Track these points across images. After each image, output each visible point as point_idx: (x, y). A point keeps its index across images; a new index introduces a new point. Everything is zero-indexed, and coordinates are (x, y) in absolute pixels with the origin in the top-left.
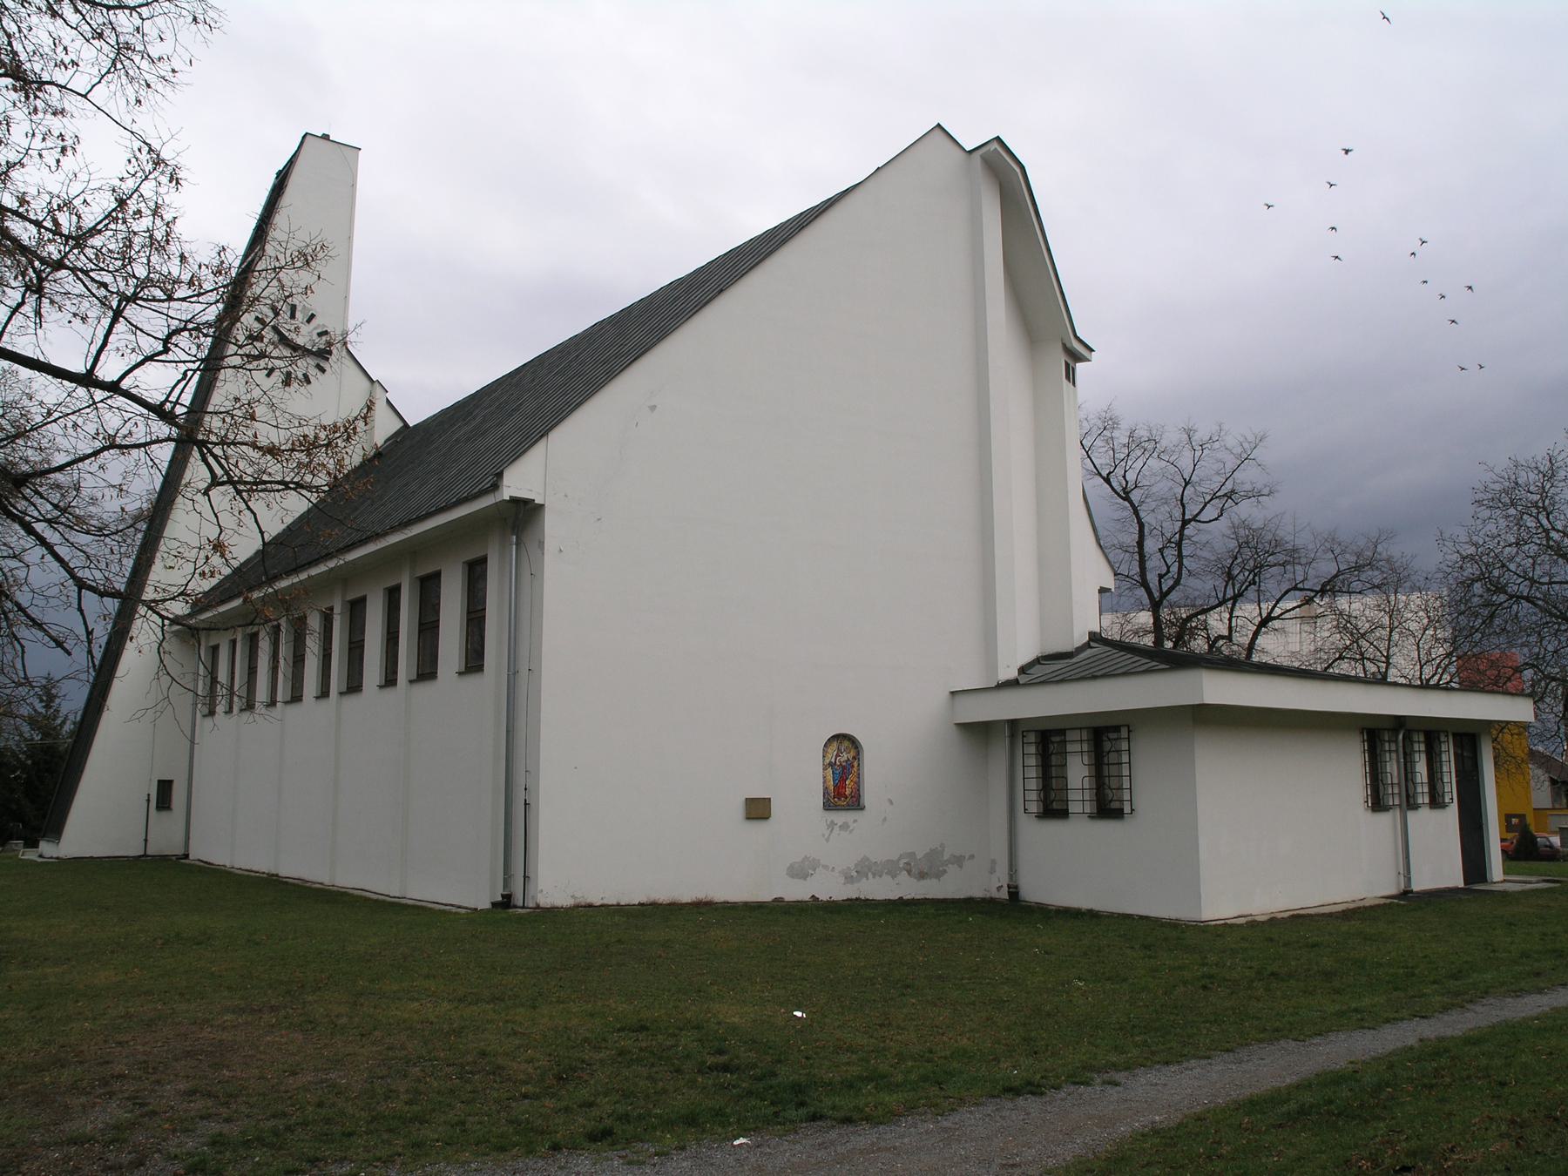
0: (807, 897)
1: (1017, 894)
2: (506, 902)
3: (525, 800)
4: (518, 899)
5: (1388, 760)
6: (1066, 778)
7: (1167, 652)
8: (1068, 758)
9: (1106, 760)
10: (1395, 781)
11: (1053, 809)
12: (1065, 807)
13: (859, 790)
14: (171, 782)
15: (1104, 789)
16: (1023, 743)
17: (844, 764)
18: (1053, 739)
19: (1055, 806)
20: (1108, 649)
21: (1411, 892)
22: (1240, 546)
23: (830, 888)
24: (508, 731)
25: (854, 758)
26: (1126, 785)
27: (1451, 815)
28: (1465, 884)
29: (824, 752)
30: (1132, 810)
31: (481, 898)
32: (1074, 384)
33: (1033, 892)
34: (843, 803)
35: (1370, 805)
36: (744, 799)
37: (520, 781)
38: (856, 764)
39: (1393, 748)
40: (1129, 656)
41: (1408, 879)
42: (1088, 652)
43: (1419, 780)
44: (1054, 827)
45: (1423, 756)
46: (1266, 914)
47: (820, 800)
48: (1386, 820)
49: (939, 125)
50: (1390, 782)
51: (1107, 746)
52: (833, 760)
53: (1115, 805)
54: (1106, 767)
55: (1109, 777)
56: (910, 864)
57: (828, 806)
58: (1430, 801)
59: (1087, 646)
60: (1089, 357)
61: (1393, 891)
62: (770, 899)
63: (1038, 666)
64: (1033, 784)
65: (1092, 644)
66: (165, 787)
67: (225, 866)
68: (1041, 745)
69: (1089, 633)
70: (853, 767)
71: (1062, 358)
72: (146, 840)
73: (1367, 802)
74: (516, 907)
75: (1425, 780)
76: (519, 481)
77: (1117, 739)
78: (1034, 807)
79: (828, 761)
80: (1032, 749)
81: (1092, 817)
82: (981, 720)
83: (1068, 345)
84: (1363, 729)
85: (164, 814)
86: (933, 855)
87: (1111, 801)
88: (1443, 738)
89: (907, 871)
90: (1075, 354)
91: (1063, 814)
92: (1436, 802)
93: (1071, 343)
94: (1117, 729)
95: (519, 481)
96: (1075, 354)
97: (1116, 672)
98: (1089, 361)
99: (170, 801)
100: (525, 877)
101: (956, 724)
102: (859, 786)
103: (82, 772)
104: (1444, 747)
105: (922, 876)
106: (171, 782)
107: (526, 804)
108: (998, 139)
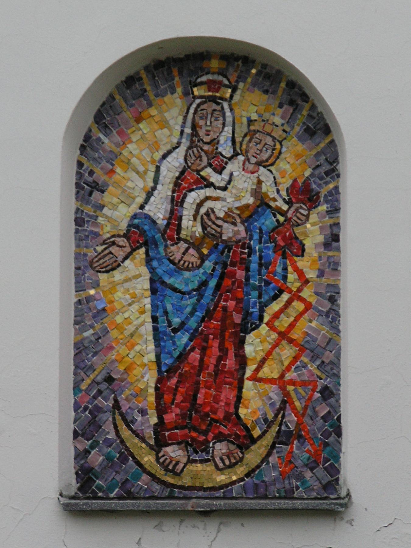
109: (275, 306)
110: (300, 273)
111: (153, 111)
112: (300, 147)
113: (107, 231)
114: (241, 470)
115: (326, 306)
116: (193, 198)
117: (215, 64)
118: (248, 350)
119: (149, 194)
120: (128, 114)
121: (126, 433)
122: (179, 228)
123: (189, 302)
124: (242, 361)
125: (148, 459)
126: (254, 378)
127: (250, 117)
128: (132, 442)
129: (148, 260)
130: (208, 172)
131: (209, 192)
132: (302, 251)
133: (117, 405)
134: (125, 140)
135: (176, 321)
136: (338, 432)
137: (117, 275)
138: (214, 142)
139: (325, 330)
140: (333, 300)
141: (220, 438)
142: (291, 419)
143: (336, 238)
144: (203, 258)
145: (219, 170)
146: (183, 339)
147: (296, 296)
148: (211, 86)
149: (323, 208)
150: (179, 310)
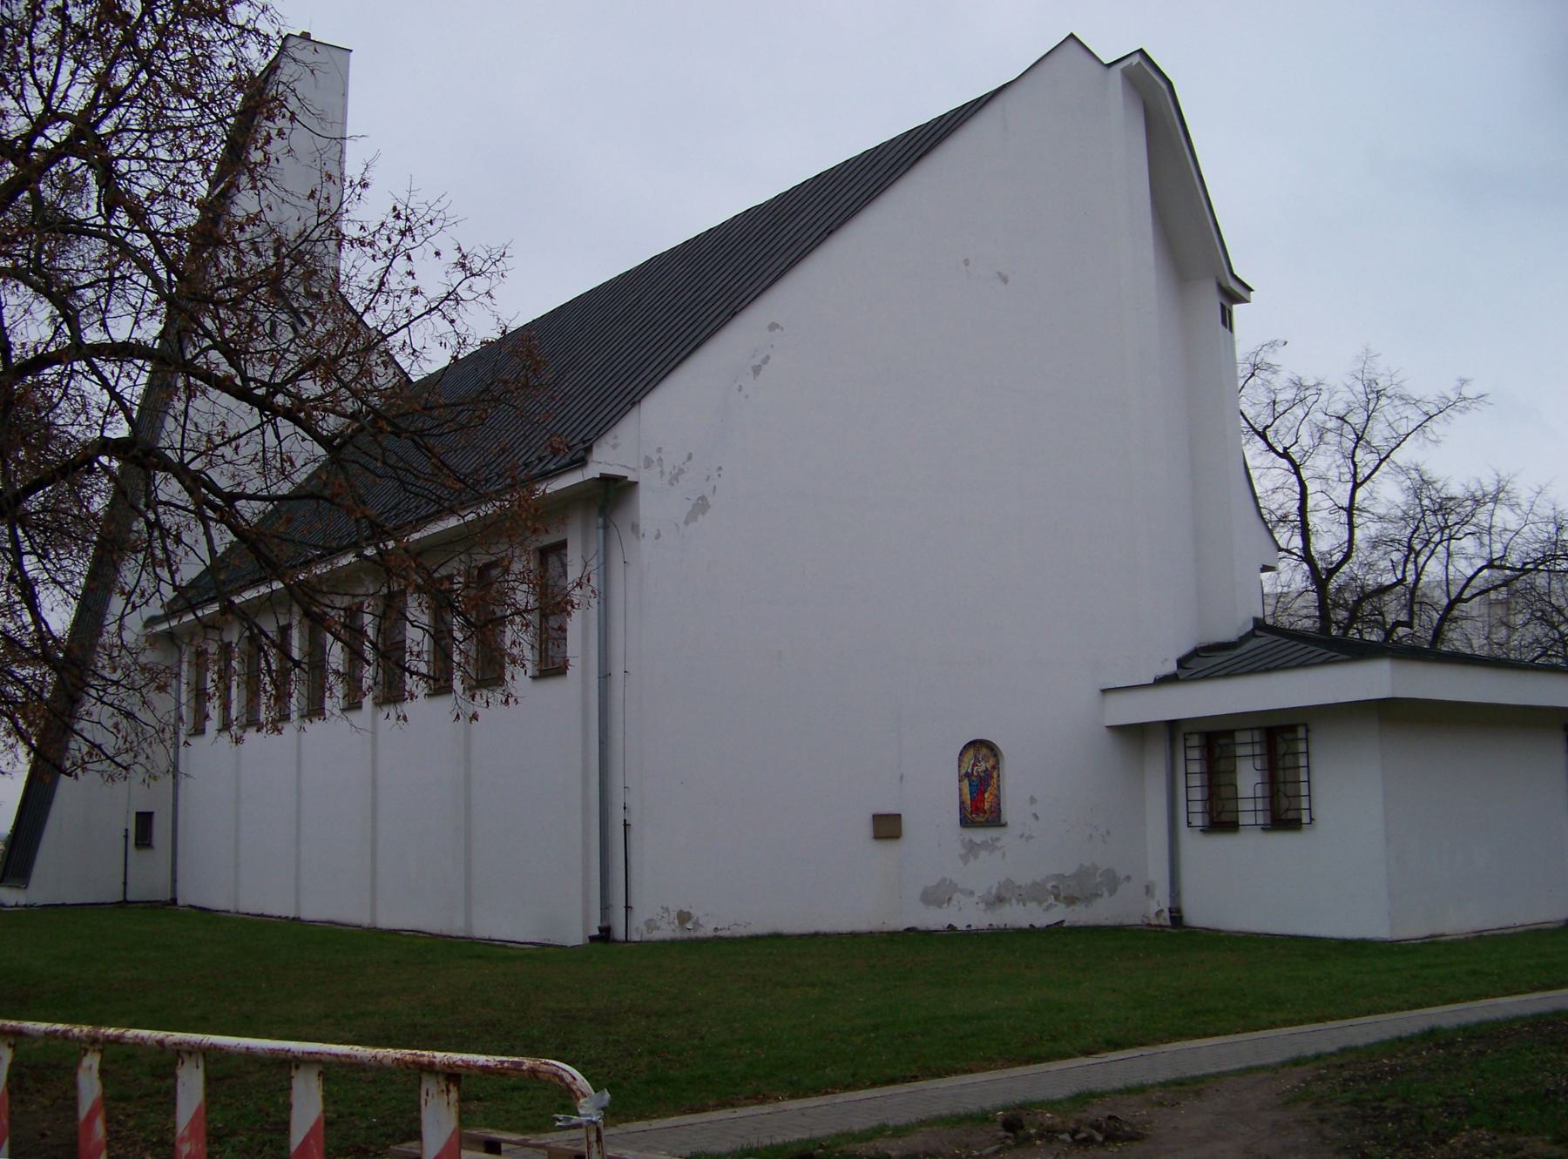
0: (1026, 925)
1: (1181, 918)
2: (605, 935)
3: (625, 821)
4: (619, 933)
7: (1335, 638)
9: (1280, 764)
11: (1221, 821)
13: (999, 804)
14: (151, 814)
16: (1185, 747)
17: (982, 774)
19: (1225, 818)
20: (1275, 638)
23: (968, 915)
24: (601, 742)
25: (994, 767)
29: (960, 760)
30: (1312, 819)
31: (574, 933)
32: (1231, 330)
33: (1196, 915)
34: (981, 819)
36: (870, 816)
37: (617, 798)
38: (995, 775)
40: (1302, 646)
42: (1254, 643)
44: (1222, 843)
47: (956, 816)
49: (1072, 36)
51: (1282, 748)
52: (969, 771)
53: (1291, 815)
54: (1281, 773)
57: (965, 822)
59: (1251, 635)
60: (1246, 298)
63: (1196, 660)
64: (1197, 794)
65: (1258, 633)
66: (145, 820)
67: (228, 912)
70: (992, 777)
71: (1214, 300)
72: (125, 883)
74: (615, 941)
76: (606, 460)
78: (1198, 820)
79: (963, 771)
80: (1195, 754)
82: (1133, 722)
83: (1224, 285)
85: (145, 853)
87: (1288, 810)
89: (1054, 894)
90: (1233, 293)
91: (1231, 826)
93: (1227, 283)
94: (1292, 728)
95: (606, 460)
96: (1233, 293)
97: (1289, 664)
98: (1247, 302)
99: (151, 837)
100: (627, 907)
103: (50, 803)
105: (1071, 901)
106: (151, 814)
107: (625, 825)
108: (1141, 51)
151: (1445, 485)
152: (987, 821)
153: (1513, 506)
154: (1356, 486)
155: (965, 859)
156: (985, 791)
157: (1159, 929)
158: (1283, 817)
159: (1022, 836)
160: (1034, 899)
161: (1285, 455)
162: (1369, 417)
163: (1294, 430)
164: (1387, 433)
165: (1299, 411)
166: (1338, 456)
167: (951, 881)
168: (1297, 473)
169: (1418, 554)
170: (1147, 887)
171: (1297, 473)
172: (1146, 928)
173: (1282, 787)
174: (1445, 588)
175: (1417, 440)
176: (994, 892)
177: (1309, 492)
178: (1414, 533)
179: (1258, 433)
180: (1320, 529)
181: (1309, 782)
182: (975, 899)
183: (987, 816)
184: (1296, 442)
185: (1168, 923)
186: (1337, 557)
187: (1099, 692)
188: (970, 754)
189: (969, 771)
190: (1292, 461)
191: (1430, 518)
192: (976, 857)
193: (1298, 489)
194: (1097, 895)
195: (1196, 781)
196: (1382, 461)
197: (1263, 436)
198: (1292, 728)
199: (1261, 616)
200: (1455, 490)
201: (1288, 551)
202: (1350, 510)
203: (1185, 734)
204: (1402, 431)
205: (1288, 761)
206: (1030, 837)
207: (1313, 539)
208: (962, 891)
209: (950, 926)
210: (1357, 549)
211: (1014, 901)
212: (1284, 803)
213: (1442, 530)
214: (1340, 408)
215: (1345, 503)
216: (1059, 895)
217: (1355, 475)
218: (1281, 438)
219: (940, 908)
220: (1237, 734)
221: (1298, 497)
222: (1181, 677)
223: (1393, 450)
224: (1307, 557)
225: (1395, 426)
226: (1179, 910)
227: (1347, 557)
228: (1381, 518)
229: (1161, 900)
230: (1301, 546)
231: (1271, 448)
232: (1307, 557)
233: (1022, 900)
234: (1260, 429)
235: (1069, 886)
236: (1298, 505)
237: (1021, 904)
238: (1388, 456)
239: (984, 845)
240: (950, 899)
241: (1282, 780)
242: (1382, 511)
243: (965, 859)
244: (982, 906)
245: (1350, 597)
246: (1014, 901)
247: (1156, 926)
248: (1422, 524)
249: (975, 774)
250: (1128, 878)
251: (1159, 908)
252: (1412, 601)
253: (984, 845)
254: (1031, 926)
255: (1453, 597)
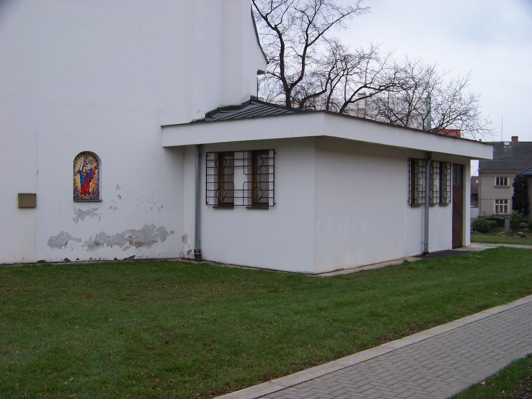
0: (112, 258)
1: (200, 255)
5: (421, 177)
6: (233, 183)
8: (235, 170)
9: (259, 172)
10: (424, 190)
12: (231, 202)
13: (98, 189)
15: (257, 190)
16: (207, 160)
17: (88, 172)
18: (226, 158)
19: (226, 200)
21: (428, 253)
22: (336, 61)
25: (96, 168)
26: (271, 187)
27: (449, 209)
28: (453, 248)
30: (274, 204)
34: (87, 197)
35: (410, 203)
38: (96, 172)
39: (424, 170)
41: (426, 245)
42: (250, 107)
43: (435, 190)
44: (224, 214)
45: (438, 176)
46: (352, 269)
48: (418, 212)
50: (421, 190)
51: (260, 163)
52: (81, 169)
53: (263, 200)
54: (259, 177)
55: (260, 182)
56: (132, 237)
57: (77, 199)
58: (440, 202)
59: (249, 103)
61: (419, 252)
62: (35, 261)
63: (218, 114)
64: (212, 187)
65: (252, 102)
68: (218, 162)
69: (251, 96)
70: (95, 173)
73: (409, 201)
75: (438, 190)
77: (266, 158)
78: (212, 201)
79: (77, 170)
80: (212, 164)
81: (249, 208)
84: (409, 158)
86: (147, 230)
87: (261, 198)
88: (448, 167)
91: (230, 206)
92: (442, 203)
94: (267, 152)
101: (167, 148)
102: (98, 186)
104: (448, 172)
105: (139, 244)
109: (93, 180)
110: (95, 176)
111: (81, 158)
112: (95, 163)
113: (76, 172)
114: (90, 197)
115: (98, 180)
116: (84, 168)
117: (87, 154)
118: (90, 184)
119: (80, 167)
120: (78, 158)
121: (78, 193)
122: (83, 171)
123: (84, 179)
124: (89, 185)
125: (80, 196)
126: (91, 187)
127: (517, 137)
128: (78, 194)
129: (80, 174)
130: (86, 165)
131: (86, 167)
132: (95, 174)
133: (77, 190)
134: (78, 161)
135: (83, 181)
136: (99, 193)
137: (77, 176)
138: (87, 162)
139: (98, 182)
140: (99, 179)
141: (87, 194)
142: (94, 191)
143: (99, 173)
144: (85, 174)
145: (87, 165)
146: (83, 183)
147: (95, 179)
148: (86, 156)
149: (97, 169)
150: (83, 180)
151: (347, 48)
152: (91, 198)
153: (377, 60)
154: (307, 46)
155: (76, 220)
156: (90, 181)
157: (188, 261)
158: (259, 201)
159: (111, 208)
160: (118, 243)
161: (275, 28)
162: (316, 13)
163: (280, 17)
164: (323, 22)
165: (283, 7)
166: (300, 31)
167: (67, 233)
168: (280, 37)
169: (332, 81)
170: (183, 237)
171: (280, 37)
172: (180, 260)
173: (259, 184)
174: (344, 96)
175: (336, 26)
176: (93, 239)
177: (285, 47)
178: (332, 69)
179: (263, 17)
180: (289, 65)
181: (274, 182)
182: (82, 243)
183: (90, 196)
184: (281, 22)
185: (194, 258)
186: (296, 79)
187: (159, 128)
188: (82, 159)
189: (81, 169)
190: (278, 32)
191: (339, 64)
192: (83, 219)
193: (280, 45)
194: (154, 242)
195: (212, 179)
196: (319, 35)
197: (266, 19)
198: (267, 152)
199: (256, 96)
200: (352, 51)
201: (274, 74)
202: (303, 57)
203: (207, 153)
204: (330, 22)
205: (263, 170)
206: (116, 208)
207: (285, 70)
208: (74, 239)
209: (66, 259)
210: (306, 75)
211: (105, 245)
212: (260, 194)
213: (344, 70)
214: (302, 7)
215: (301, 54)
216: (132, 241)
217: (307, 41)
218: (274, 20)
219: (61, 249)
220: (235, 153)
221: (280, 49)
222: (206, 120)
223: (325, 30)
224: (282, 77)
225: (327, 19)
226: (200, 251)
227: (300, 79)
228: (317, 62)
229: (190, 245)
230: (280, 72)
231: (270, 25)
232: (282, 77)
233: (110, 244)
234: (265, 15)
235: (138, 236)
236: (280, 53)
237: (110, 247)
238: (323, 33)
239: (88, 213)
240: (66, 244)
241: (259, 181)
242: (318, 58)
243: (76, 220)
244: (86, 248)
245: (300, 97)
246: (105, 245)
247: (187, 259)
248: (335, 66)
249: (84, 171)
250: (173, 232)
251: (190, 249)
252: (328, 102)
253: (88, 213)
254: (115, 259)
255: (347, 100)
